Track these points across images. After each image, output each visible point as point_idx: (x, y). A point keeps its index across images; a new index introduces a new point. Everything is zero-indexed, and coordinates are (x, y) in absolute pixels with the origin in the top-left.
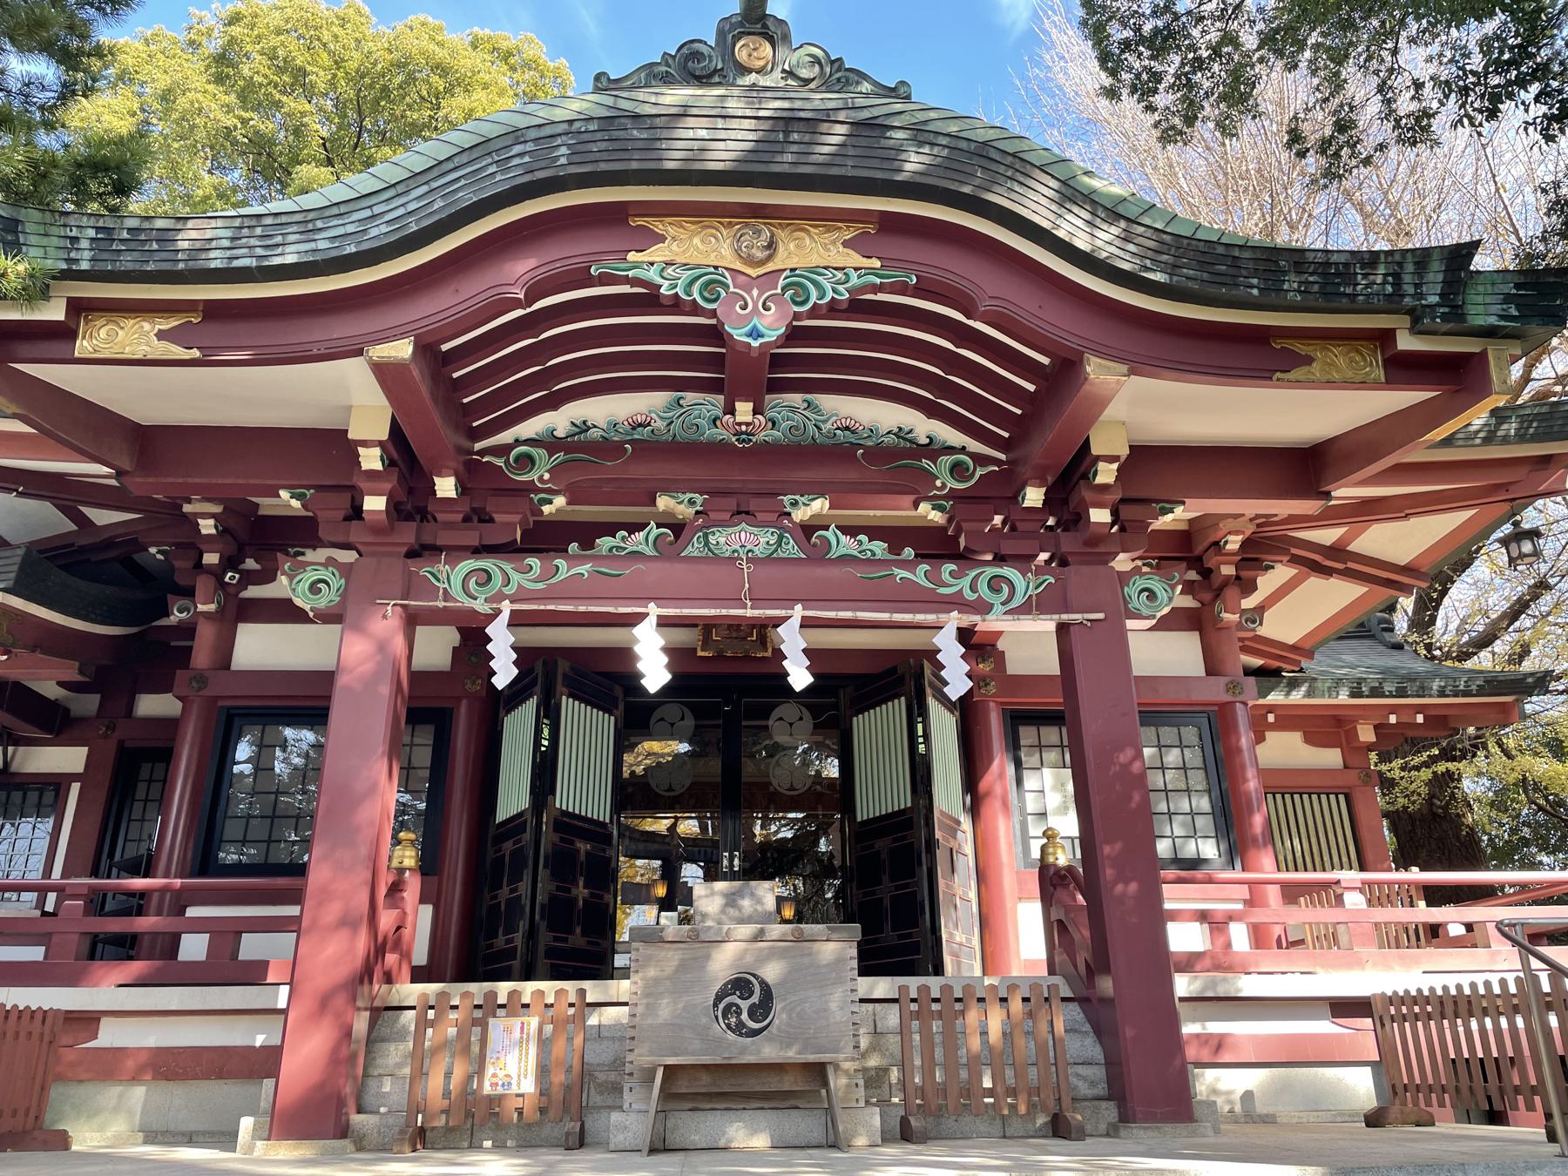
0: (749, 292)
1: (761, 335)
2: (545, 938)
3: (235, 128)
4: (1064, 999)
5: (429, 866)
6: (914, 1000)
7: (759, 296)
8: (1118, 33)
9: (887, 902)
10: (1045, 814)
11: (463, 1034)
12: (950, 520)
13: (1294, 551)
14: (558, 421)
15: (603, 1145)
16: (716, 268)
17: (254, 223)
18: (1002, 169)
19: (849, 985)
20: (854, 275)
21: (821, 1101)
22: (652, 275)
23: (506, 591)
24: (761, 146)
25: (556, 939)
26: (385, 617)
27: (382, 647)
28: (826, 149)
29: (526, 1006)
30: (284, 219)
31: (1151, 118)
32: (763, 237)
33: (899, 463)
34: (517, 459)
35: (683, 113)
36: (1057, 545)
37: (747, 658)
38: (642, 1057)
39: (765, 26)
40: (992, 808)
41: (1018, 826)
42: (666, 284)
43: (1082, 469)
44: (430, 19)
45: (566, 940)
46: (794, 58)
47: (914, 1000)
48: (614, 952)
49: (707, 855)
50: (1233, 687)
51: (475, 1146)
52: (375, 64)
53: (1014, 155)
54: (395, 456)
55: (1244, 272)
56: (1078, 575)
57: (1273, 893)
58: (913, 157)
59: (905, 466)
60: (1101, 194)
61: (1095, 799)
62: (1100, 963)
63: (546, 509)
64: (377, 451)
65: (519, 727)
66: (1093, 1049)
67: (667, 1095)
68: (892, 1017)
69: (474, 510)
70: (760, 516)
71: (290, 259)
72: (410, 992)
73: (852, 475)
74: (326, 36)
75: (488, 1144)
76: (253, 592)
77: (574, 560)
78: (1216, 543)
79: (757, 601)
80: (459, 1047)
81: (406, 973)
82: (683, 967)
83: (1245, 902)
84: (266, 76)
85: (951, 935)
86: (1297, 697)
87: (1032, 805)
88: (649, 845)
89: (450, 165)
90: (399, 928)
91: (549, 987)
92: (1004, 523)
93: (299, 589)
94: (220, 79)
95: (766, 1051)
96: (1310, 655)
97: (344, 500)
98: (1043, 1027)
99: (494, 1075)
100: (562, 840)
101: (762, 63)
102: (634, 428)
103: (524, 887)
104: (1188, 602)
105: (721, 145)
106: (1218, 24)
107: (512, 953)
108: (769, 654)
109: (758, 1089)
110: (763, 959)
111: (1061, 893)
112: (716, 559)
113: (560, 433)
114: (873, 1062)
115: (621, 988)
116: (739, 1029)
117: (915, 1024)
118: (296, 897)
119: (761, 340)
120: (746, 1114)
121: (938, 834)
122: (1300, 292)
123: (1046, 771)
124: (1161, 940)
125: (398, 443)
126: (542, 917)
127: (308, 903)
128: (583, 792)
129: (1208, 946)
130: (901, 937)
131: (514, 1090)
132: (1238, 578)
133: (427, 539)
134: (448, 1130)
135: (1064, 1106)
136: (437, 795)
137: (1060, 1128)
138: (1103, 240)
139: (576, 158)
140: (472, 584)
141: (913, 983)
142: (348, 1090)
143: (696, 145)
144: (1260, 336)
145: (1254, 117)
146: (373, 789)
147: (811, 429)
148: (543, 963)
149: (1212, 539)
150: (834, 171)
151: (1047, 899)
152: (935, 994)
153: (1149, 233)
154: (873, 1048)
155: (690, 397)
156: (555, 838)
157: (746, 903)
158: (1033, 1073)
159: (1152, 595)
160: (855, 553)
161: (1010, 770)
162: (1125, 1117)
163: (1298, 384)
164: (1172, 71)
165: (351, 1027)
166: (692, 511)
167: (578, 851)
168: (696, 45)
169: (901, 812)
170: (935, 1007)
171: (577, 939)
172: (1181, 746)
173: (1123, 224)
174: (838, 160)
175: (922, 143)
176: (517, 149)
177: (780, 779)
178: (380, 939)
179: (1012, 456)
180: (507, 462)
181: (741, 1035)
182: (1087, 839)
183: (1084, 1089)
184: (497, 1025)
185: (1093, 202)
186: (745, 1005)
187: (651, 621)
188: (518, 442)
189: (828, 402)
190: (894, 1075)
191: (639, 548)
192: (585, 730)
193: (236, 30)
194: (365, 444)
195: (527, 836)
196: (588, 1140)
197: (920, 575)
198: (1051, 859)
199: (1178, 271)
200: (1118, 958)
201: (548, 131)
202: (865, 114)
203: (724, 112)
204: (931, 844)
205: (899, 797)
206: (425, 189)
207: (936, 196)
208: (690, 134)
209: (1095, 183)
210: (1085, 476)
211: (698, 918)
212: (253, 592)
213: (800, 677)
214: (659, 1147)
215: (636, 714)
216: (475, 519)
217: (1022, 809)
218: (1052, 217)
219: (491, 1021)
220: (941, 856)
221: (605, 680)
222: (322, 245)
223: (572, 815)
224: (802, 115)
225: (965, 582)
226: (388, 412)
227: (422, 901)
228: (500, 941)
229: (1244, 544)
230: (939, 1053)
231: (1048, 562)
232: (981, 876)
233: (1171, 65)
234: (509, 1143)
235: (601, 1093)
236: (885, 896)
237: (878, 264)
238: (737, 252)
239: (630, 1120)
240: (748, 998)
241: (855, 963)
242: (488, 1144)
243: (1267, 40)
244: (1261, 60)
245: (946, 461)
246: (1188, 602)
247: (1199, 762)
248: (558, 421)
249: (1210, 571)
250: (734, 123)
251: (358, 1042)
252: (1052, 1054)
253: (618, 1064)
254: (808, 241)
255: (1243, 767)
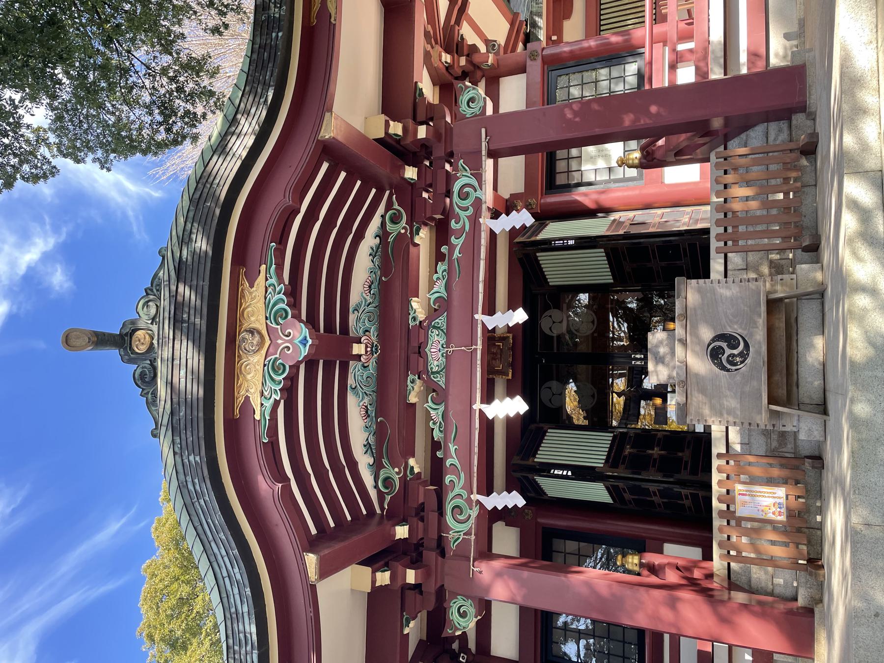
0: (279, 345)
1: (305, 338)
2: (684, 475)
3: (211, 640)
4: (725, 148)
5: (640, 548)
6: (726, 244)
7: (281, 339)
8: (161, 136)
9: (663, 264)
10: (610, 168)
11: (747, 532)
12: (426, 225)
13: (452, 22)
14: (364, 461)
15: (820, 445)
16: (265, 365)
17: (232, 651)
18: (206, 190)
19: (716, 285)
20: (270, 281)
21: (791, 303)
22: (269, 404)
23: (465, 497)
24: (191, 337)
25: (686, 468)
26: (481, 572)
27: (498, 575)
28: (193, 297)
29: (728, 492)
30: (230, 632)
31: (210, 116)
32: (247, 337)
33: (394, 259)
34: (386, 488)
35: (170, 384)
36: (440, 158)
37: (513, 348)
38: (762, 419)
39: (126, 334)
40: (606, 200)
41: (617, 185)
42: (274, 396)
43: (394, 143)
44: (154, 525)
45: (686, 463)
46: (144, 317)
47: (726, 244)
48: (694, 432)
49: (638, 374)
50: (533, 56)
51: (821, 527)
52: (177, 559)
53: (198, 183)
54: (382, 563)
55: (269, 41)
56: (458, 147)
57: (658, 29)
58: (198, 244)
59: (392, 252)
60: (221, 130)
61: (598, 131)
62: (702, 128)
63: (416, 470)
64: (379, 575)
65: (555, 487)
66: (759, 130)
67: (788, 402)
68: (735, 259)
69: (417, 515)
70: (422, 340)
71: (254, 629)
72: (718, 564)
73: (398, 284)
74: (161, 586)
75: (819, 518)
76: (472, 645)
77: (447, 455)
78: (447, 68)
79: (473, 342)
80: (754, 536)
81: (706, 564)
82: (703, 391)
83: (665, 45)
84: (182, 622)
85: (684, 224)
86: (541, 22)
87: (605, 177)
88: (631, 411)
89: (199, 528)
90: (678, 568)
91: (716, 477)
92: (427, 191)
93: (464, 624)
94: (185, 648)
95: (759, 337)
96: (516, 15)
97: (410, 594)
98: (742, 161)
99: (774, 513)
100: (623, 463)
101: (147, 337)
102: (369, 416)
103: (653, 487)
104: (482, 84)
105: (190, 362)
106: (158, 79)
107: (694, 497)
108: (511, 335)
109: (784, 344)
110: (699, 341)
111: (658, 155)
112: (447, 368)
113: (371, 461)
114: (765, 270)
115: (717, 431)
116: (744, 356)
117: (741, 243)
118: (658, 637)
119: (308, 338)
120: (801, 351)
121: (621, 232)
122: (280, 7)
123: (583, 169)
124: (687, 87)
125: (374, 561)
126: (671, 477)
127: (660, 628)
128: (594, 450)
129: (692, 63)
130: (685, 255)
131: (783, 501)
132: (468, 55)
133: (434, 544)
134: (809, 543)
135: (795, 147)
136: (595, 539)
137: (810, 150)
138: (249, 128)
139: (197, 451)
140: (460, 517)
141: (714, 244)
142: (782, 607)
143: (189, 377)
144: (309, 33)
145: (210, 57)
146: (588, 584)
147: (370, 308)
148: (700, 477)
149: (444, 71)
150: (206, 293)
151: (662, 163)
152: (721, 230)
153: (244, 100)
154: (756, 270)
155: (351, 381)
156: (622, 467)
157: (662, 350)
158: (773, 167)
159: (472, 100)
160: (444, 282)
161: (582, 189)
162: (802, 108)
163: (339, 8)
164: (183, 104)
165: (741, 604)
166: (418, 382)
167: (630, 453)
168: (136, 376)
169: (607, 255)
170: (730, 230)
171: (685, 455)
172: (569, 87)
173: (239, 116)
174: (199, 290)
175: (190, 239)
176: (190, 487)
177: (587, 329)
178: (683, 582)
179: (387, 187)
180: (388, 494)
181: (748, 354)
182: (624, 136)
183: (784, 136)
184: (741, 511)
185: (226, 134)
186: (728, 352)
187: (484, 407)
188: (376, 487)
189: (355, 298)
190: (774, 256)
191: (440, 414)
192: (556, 447)
193: (157, 637)
194: (374, 581)
195: (621, 485)
196: (816, 454)
197: (457, 242)
198: (636, 161)
199: (267, 82)
200: (697, 115)
201: (180, 468)
202: (173, 273)
203: (170, 360)
204: (627, 236)
205: (598, 256)
206: (213, 544)
207: (224, 234)
208: (183, 380)
209: (215, 134)
210: (398, 142)
211: (671, 381)
212: (472, 645)
213: (520, 316)
214: (823, 408)
215: (543, 417)
216: (422, 514)
217: (606, 182)
218: (234, 159)
219: (738, 514)
220: (634, 230)
221: (526, 434)
222: (245, 609)
223: (608, 456)
224: (172, 312)
225: (462, 214)
226: (354, 566)
227: (660, 551)
228: (687, 503)
229: (447, 51)
230: (759, 228)
231: (451, 164)
232: (648, 207)
233: (180, 104)
234: (818, 504)
235: (786, 444)
236: (657, 264)
237: (263, 267)
238: (255, 352)
239: (804, 428)
240: (723, 349)
241: (701, 281)
242: (819, 518)
243: (167, 49)
244: (178, 54)
245: (389, 226)
246: (482, 84)
247: (578, 75)
248: (364, 461)
249: (463, 72)
250: (177, 354)
251: (750, 600)
252: (761, 155)
253: (766, 433)
254: (249, 309)
255: (582, 49)
